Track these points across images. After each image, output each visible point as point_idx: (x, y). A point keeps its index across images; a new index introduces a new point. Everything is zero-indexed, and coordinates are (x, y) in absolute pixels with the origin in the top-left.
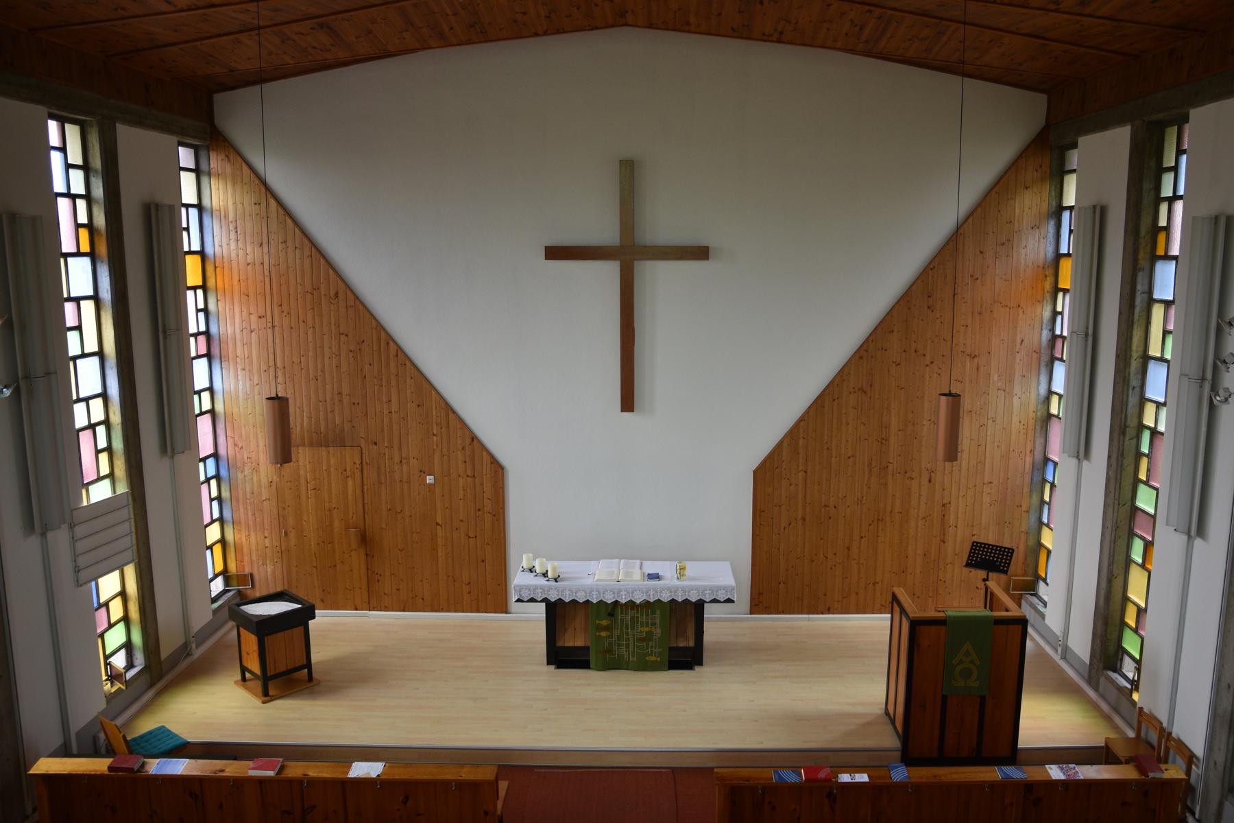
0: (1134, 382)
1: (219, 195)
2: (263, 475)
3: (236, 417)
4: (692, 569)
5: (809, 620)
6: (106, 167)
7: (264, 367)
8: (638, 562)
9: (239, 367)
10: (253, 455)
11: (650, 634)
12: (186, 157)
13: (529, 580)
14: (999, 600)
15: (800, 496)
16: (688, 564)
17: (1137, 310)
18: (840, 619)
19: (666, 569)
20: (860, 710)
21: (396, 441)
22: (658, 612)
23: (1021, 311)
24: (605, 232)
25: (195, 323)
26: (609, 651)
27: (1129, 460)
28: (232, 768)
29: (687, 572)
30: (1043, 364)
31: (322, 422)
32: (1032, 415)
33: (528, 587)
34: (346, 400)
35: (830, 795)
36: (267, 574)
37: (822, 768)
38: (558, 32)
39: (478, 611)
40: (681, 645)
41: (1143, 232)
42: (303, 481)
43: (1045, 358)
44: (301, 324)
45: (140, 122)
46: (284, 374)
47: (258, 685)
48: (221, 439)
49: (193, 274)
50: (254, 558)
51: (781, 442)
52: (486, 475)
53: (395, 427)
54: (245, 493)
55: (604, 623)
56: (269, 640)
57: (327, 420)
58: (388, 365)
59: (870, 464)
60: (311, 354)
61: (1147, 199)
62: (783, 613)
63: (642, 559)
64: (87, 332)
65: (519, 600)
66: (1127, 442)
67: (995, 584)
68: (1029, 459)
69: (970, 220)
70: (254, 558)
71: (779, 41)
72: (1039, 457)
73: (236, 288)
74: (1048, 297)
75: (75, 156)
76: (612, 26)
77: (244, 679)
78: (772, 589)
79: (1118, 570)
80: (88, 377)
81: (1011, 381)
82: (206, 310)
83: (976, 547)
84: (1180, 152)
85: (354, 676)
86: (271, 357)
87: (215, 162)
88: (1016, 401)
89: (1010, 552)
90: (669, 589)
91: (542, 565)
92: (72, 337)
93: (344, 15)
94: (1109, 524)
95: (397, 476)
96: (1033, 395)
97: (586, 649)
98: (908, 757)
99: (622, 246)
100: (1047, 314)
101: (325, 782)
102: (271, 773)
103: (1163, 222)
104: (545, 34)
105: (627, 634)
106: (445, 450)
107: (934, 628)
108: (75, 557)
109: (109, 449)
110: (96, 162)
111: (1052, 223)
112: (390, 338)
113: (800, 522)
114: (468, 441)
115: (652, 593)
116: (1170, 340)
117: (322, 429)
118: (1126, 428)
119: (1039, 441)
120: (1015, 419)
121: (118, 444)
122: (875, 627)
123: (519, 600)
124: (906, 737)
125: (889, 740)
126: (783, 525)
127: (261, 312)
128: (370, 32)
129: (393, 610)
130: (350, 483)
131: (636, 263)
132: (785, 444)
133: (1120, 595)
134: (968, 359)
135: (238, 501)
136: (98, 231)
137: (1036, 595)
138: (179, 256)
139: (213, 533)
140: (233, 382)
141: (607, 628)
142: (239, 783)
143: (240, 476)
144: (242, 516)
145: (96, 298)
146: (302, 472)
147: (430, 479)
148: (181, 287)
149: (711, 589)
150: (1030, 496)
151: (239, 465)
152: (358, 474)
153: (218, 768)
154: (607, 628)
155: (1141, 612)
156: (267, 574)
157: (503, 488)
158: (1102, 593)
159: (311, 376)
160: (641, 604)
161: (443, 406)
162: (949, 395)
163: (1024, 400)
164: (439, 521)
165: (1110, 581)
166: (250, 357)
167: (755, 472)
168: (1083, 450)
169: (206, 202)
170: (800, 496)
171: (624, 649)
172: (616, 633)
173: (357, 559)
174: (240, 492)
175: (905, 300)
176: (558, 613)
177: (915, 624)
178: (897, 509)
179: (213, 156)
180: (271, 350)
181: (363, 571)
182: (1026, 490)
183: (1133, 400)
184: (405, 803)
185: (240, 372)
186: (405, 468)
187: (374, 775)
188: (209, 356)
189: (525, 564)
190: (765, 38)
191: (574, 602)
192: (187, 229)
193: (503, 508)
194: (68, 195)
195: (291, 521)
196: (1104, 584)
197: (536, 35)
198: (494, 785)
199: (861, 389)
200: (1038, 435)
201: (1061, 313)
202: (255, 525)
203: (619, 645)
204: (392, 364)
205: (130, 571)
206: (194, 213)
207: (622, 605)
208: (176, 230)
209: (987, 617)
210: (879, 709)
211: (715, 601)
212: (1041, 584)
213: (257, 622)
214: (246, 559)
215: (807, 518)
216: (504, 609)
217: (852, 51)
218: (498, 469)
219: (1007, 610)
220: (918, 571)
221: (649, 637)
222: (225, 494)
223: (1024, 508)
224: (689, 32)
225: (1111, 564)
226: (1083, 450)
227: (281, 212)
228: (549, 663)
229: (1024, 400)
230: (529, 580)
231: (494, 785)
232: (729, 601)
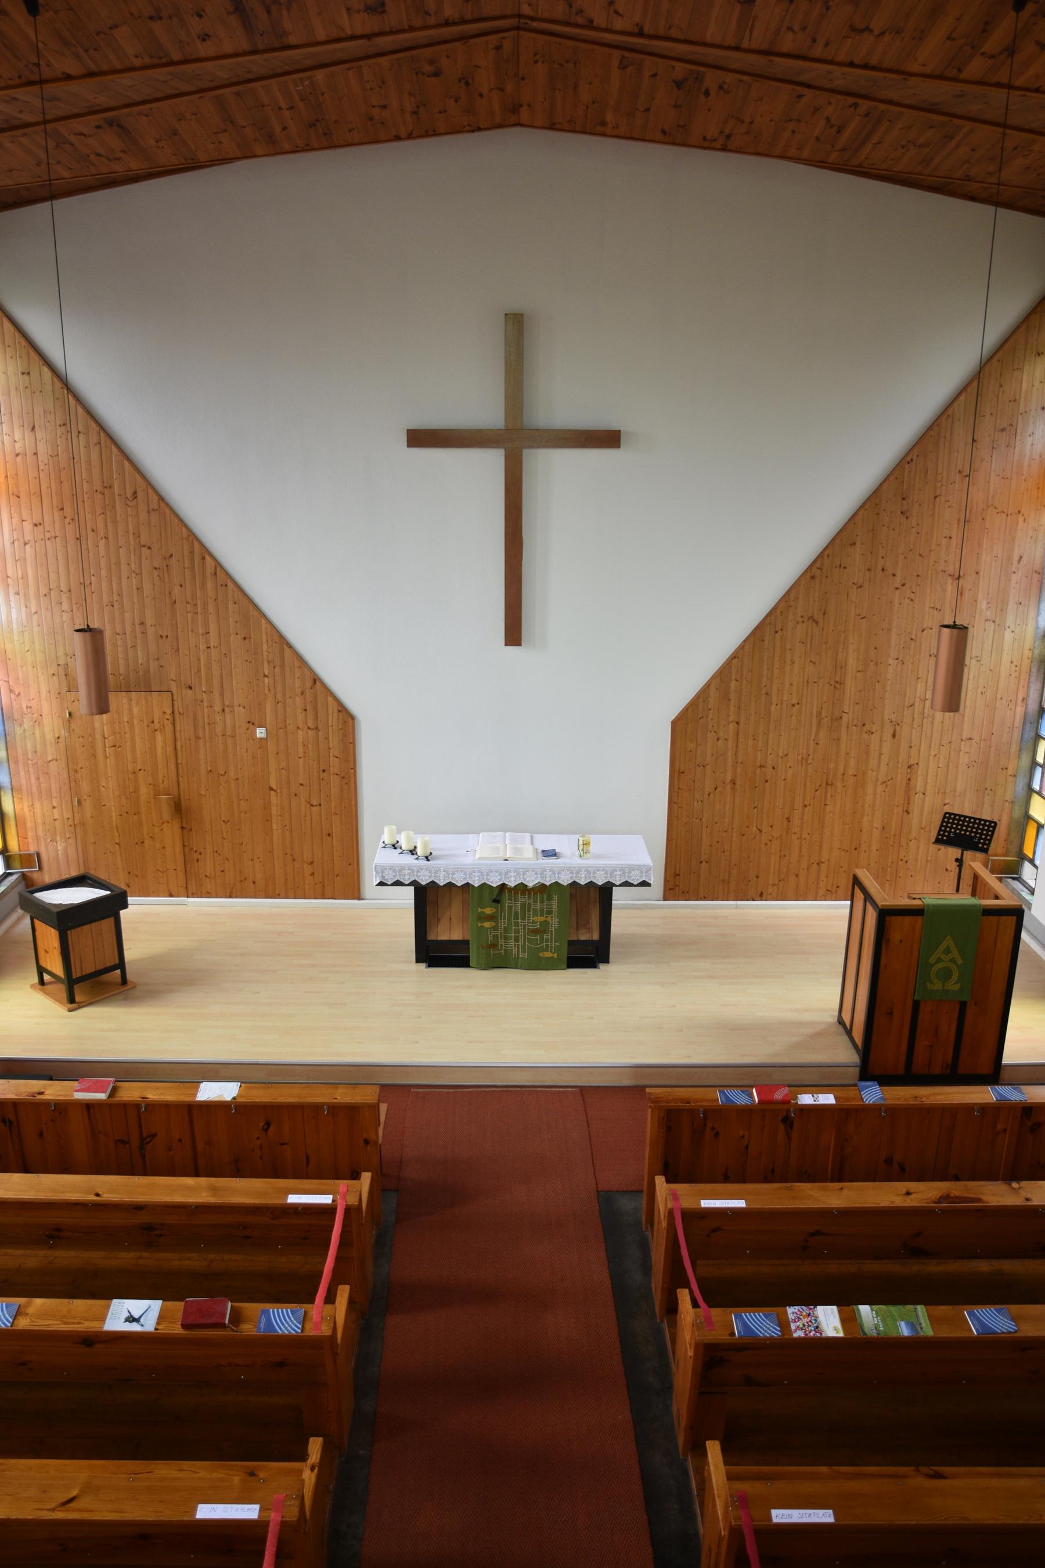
2: (47, 729)
3: (9, 655)
4: (599, 844)
5: (737, 907)
7: (43, 590)
8: (527, 836)
9: (12, 591)
10: (34, 703)
13: (393, 858)
14: (985, 884)
15: (730, 753)
16: (593, 839)
18: (775, 907)
19: (565, 845)
20: (808, 1017)
22: (555, 897)
23: (1021, 519)
24: (486, 410)
26: (494, 946)
28: (53, 1091)
29: (592, 848)
31: (121, 661)
32: (1027, 653)
33: (392, 868)
34: (151, 631)
35: (787, 1120)
36: (58, 854)
37: (778, 1087)
38: (426, 135)
39: (323, 897)
40: (583, 938)
42: (99, 737)
44: (90, 534)
46: (70, 599)
47: (62, 990)
50: (40, 833)
51: (708, 685)
52: (333, 728)
53: (215, 666)
54: (25, 753)
55: (488, 911)
56: (72, 935)
57: (126, 659)
58: (203, 587)
59: (819, 714)
60: (104, 573)
62: (705, 898)
63: (533, 832)
67: (975, 862)
68: (1020, 710)
69: (962, 398)
70: (40, 833)
71: (724, 149)
76: (500, 126)
77: (42, 982)
78: (690, 872)
81: (1003, 611)
83: (949, 819)
85: (178, 978)
86: (53, 576)
88: (1008, 636)
89: (992, 825)
90: (570, 869)
91: (409, 839)
93: (141, 108)
95: (219, 730)
97: (465, 944)
98: (867, 1073)
99: (508, 430)
101: (167, 1106)
102: (102, 1096)
104: (410, 137)
106: (279, 696)
107: (907, 919)
112: (206, 552)
113: (728, 787)
115: (548, 874)
117: (122, 670)
120: (1006, 659)
122: (830, 917)
123: (381, 884)
124: (866, 1052)
125: (846, 1055)
126: (707, 789)
127: (37, 519)
128: (175, 133)
129: (217, 897)
130: (159, 738)
131: (525, 452)
132: (713, 688)
134: (950, 580)
135: (17, 762)
137: (1019, 879)
141: (491, 918)
142: (62, 1108)
143: (19, 731)
144: (23, 781)
147: (260, 733)
149: (622, 869)
150: (1019, 756)
151: (16, 716)
152: (169, 728)
153: (37, 1090)
154: (491, 918)
156: (58, 854)
157: (353, 743)
159: (105, 601)
160: (533, 888)
161: (276, 638)
162: (954, 626)
166: (24, 577)
167: (674, 723)
170: (730, 753)
171: (512, 943)
172: (503, 923)
173: (171, 833)
174: (20, 751)
175: (873, 503)
176: (428, 898)
177: (885, 915)
178: (851, 772)
180: (52, 568)
181: (178, 848)
182: (1014, 748)
184: (266, 1130)
185: (12, 597)
187: (228, 1097)
189: (387, 838)
190: (706, 144)
191: (450, 885)
193: (354, 768)
195: (85, 786)
197: (398, 138)
198: (375, 1108)
199: (811, 618)
200: (1033, 679)
202: (40, 792)
203: (506, 938)
204: (210, 585)
207: (511, 889)
209: (974, 906)
210: (831, 1017)
212: (1027, 867)
213: (59, 913)
214: (30, 834)
215: (738, 782)
216: (354, 892)
217: (821, 164)
218: (347, 719)
219: (997, 898)
220: (874, 848)
223: (1010, 771)
224: (604, 135)
227: (58, 384)
228: (418, 961)
230: (393, 858)
231: (375, 1108)
232: (644, 884)
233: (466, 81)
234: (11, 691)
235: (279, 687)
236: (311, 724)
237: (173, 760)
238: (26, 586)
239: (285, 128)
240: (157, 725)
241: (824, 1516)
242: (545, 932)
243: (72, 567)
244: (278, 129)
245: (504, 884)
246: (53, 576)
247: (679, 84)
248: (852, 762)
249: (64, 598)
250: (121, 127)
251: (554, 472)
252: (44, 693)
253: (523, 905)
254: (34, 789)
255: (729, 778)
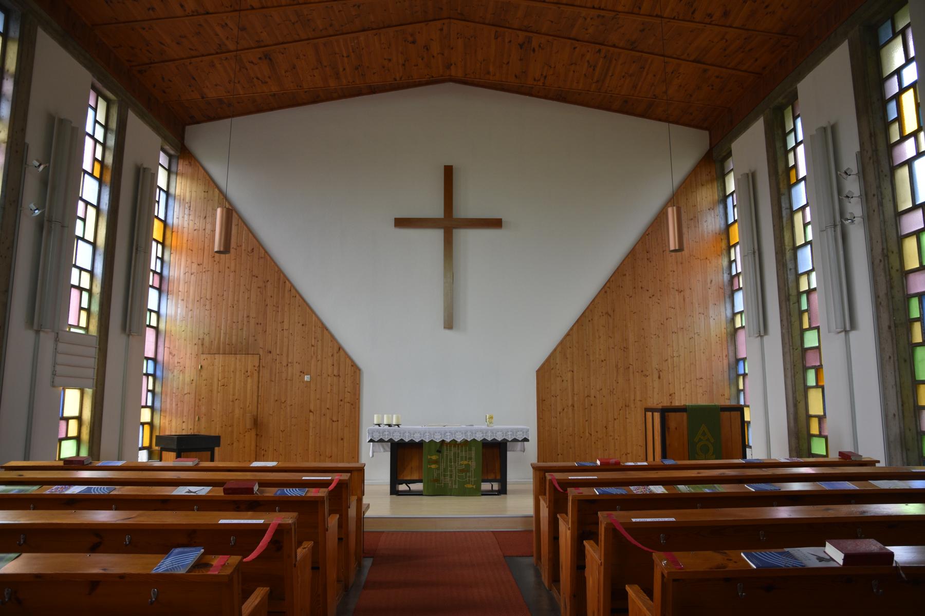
0: (790, 265)
1: (180, 187)
6: (119, 131)
7: (197, 298)
9: (180, 298)
11: (468, 466)
12: (163, 159)
17: (785, 220)
21: (285, 349)
22: (473, 448)
25: (155, 265)
27: (795, 318)
30: (727, 296)
32: (724, 331)
34: (252, 321)
41: (780, 172)
42: (216, 380)
43: (728, 292)
45: (142, 116)
48: (160, 350)
49: (157, 233)
53: (285, 340)
55: (434, 457)
59: (617, 366)
61: (780, 153)
64: (89, 226)
65: (371, 441)
66: (792, 306)
68: (725, 362)
72: (732, 360)
73: (185, 245)
74: (725, 252)
75: (101, 118)
79: (800, 397)
80: (83, 255)
82: (162, 259)
84: (795, 118)
87: (182, 166)
92: (79, 223)
94: (788, 366)
96: (723, 318)
100: (725, 263)
103: (792, 163)
105: (451, 466)
108: (55, 364)
109: (88, 310)
110: (113, 125)
111: (721, 206)
113: (570, 408)
114: (336, 349)
116: (809, 228)
117: (234, 341)
118: (790, 296)
119: (731, 348)
121: (95, 308)
123: (371, 441)
130: (249, 380)
133: (805, 416)
134: (677, 293)
135: (166, 395)
136: (107, 167)
138: (152, 216)
139: (146, 416)
140: (174, 308)
141: (436, 462)
143: (170, 376)
145: (97, 208)
146: (216, 373)
147: (307, 378)
148: (149, 239)
154: (436, 462)
155: (821, 419)
158: (792, 417)
161: (320, 325)
163: (715, 321)
164: (312, 409)
165: (795, 405)
167: (538, 371)
168: (763, 329)
169: (172, 191)
171: (448, 478)
172: (443, 466)
174: (169, 389)
178: (638, 398)
179: (181, 162)
181: (253, 447)
183: (791, 277)
186: (290, 369)
188: (160, 290)
192: (158, 202)
194: (92, 137)
195: (203, 409)
196: (792, 410)
199: (607, 313)
201: (735, 261)
202: (177, 413)
205: (89, 392)
206: (163, 195)
208: (153, 202)
211: (515, 440)
218: (356, 370)
221: (466, 469)
222: (158, 389)
225: (794, 392)
226: (763, 329)
229: (715, 321)
233: (427, 48)
234: (170, 353)
235: (319, 352)
236: (335, 373)
237: (256, 394)
238: (188, 297)
239: (344, 69)
240: (249, 373)
241: (673, 519)
242: (468, 471)
243: (215, 286)
244: (341, 70)
245: (443, 441)
246: (203, 291)
247: (521, 46)
248: (638, 393)
249: (208, 302)
250: (270, 60)
251: (468, 238)
252: (188, 355)
253: (455, 454)
254: (174, 411)
255: (570, 404)
